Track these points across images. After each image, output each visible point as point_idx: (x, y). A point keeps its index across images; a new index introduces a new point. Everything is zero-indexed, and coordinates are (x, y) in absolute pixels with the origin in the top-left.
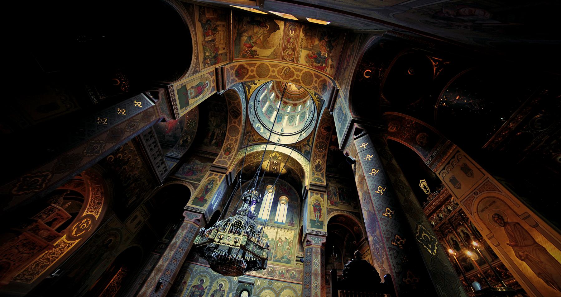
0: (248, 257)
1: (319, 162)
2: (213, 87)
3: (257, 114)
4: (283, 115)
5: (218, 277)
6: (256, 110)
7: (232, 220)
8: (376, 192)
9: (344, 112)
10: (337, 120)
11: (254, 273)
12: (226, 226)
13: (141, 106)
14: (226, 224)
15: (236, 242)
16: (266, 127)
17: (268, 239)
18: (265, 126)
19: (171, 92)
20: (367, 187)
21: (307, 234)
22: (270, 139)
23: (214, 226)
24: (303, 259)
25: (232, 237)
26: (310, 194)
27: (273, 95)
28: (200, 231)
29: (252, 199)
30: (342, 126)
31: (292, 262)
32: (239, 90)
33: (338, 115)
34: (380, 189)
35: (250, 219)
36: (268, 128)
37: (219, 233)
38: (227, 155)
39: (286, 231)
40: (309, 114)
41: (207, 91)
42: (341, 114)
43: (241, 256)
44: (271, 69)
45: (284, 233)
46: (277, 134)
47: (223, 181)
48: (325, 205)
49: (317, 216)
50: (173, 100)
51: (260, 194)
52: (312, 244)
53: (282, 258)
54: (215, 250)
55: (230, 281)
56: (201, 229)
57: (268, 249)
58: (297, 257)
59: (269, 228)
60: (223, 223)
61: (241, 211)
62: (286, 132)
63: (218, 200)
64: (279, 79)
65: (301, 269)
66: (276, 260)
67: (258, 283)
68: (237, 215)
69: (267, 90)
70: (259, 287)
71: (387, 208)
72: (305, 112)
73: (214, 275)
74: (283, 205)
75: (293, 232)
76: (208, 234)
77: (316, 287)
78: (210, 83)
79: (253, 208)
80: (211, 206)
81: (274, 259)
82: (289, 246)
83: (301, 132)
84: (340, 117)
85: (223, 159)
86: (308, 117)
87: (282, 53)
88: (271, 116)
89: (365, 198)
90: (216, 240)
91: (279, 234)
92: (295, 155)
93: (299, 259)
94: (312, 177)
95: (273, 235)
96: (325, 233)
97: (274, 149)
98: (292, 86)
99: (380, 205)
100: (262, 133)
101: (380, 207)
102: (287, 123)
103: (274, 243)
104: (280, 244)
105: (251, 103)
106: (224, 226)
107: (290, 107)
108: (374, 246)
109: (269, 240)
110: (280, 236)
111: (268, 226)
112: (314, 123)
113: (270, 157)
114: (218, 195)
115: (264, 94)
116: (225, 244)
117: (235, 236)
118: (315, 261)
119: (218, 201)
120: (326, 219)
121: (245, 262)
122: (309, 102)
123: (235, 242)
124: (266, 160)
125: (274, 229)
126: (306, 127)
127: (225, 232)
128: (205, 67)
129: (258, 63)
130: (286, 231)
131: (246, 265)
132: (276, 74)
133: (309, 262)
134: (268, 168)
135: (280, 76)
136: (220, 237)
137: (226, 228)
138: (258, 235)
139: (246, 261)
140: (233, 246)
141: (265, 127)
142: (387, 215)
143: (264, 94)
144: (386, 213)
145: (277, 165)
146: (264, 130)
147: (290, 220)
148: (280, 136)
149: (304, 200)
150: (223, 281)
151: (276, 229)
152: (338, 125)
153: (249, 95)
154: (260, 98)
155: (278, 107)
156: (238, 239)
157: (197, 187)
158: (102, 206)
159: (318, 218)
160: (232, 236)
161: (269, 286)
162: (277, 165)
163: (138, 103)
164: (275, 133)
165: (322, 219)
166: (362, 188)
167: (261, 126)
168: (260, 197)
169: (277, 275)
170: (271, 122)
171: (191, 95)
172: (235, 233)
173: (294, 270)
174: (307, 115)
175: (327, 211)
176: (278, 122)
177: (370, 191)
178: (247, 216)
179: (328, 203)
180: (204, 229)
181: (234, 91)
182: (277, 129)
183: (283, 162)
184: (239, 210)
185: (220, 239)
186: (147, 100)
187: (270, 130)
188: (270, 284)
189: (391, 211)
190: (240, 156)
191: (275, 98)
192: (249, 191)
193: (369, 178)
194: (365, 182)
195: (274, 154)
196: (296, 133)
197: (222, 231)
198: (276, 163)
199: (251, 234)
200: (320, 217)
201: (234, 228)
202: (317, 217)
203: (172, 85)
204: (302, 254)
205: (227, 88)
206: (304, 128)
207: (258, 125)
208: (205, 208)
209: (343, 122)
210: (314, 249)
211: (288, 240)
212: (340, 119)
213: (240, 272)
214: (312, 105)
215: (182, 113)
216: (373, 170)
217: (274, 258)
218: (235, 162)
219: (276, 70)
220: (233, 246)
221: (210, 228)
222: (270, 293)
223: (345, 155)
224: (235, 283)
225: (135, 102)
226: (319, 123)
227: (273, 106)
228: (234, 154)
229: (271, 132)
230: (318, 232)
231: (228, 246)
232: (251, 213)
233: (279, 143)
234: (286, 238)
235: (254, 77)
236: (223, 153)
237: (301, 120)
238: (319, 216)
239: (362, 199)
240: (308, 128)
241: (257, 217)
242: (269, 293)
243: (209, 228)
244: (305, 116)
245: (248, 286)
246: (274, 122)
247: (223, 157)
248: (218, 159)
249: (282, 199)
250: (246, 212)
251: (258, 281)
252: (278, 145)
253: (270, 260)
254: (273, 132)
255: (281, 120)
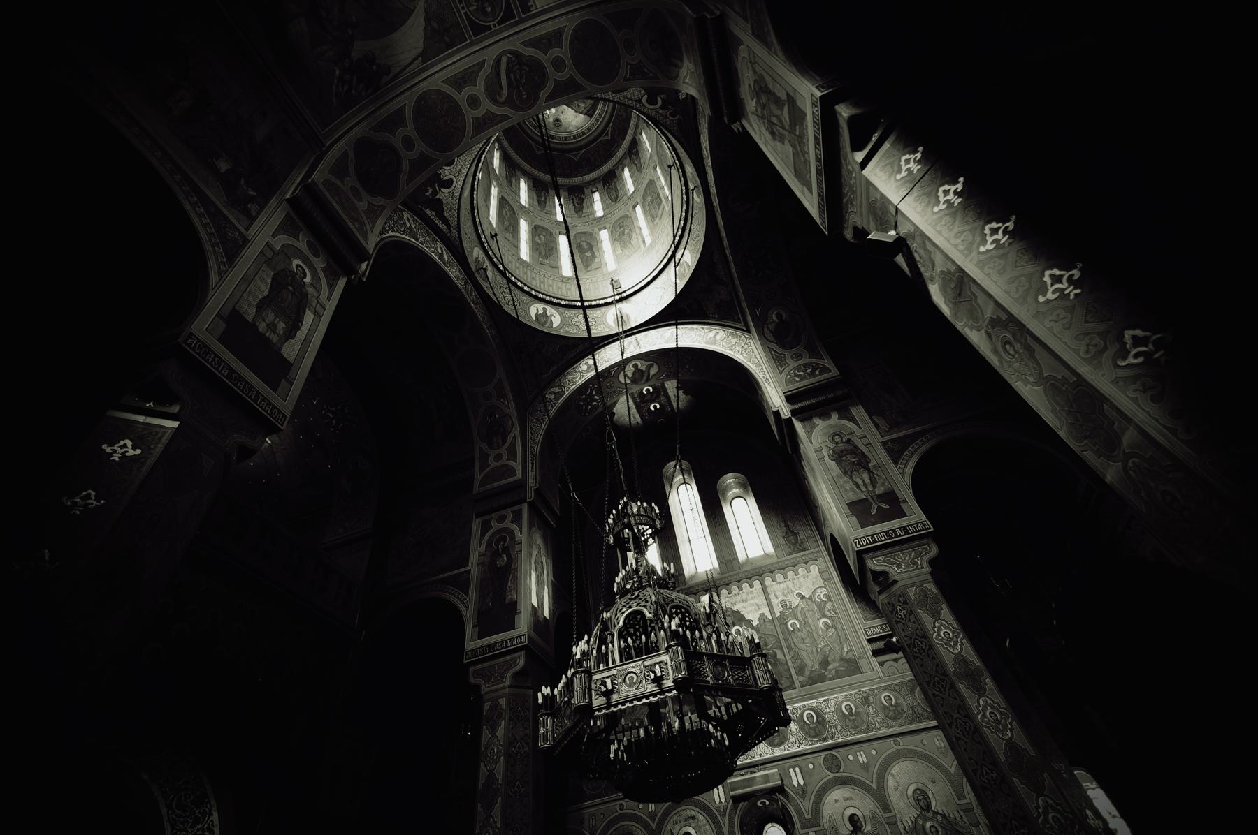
0: (719, 708)
1: (779, 316)
2: (324, 270)
3: (513, 279)
4: (591, 235)
5: (667, 813)
6: (500, 266)
7: (614, 619)
8: (1041, 299)
9: (779, 94)
10: (769, 137)
11: (762, 751)
12: (604, 647)
13: (138, 451)
14: (602, 641)
15: (658, 680)
16: (563, 302)
17: (749, 623)
18: (555, 301)
19: (204, 359)
20: (997, 303)
21: (860, 555)
22: (592, 332)
23: (573, 666)
24: (894, 640)
25: (638, 672)
26: (804, 428)
27: (523, 186)
28: (540, 701)
29: (638, 528)
30: (794, 147)
31: (863, 663)
32: (410, 232)
33: (762, 117)
34: (1055, 279)
35: (662, 591)
36: (570, 303)
37: (595, 677)
38: (499, 448)
39: (790, 574)
40: (666, 180)
41: (316, 294)
42: (773, 106)
43: (695, 717)
44: (461, 97)
45: (789, 583)
46: (606, 304)
47: (531, 525)
48: (870, 439)
49: (860, 482)
50: (229, 378)
51: (653, 504)
52: (897, 578)
53: (825, 663)
54: (612, 737)
55: (706, 809)
56: (539, 694)
57: (764, 656)
58: (869, 641)
59: (735, 589)
60: (591, 642)
61: (625, 580)
62: (627, 284)
63: (546, 584)
64: (505, 118)
65: (907, 676)
66: (810, 678)
67: (796, 779)
68: (620, 598)
69: (494, 183)
70: (802, 792)
71: (1128, 334)
72: (651, 183)
73: (652, 816)
74: (738, 502)
75: (814, 569)
76: (566, 699)
77: (997, 722)
78: (305, 259)
79: (653, 555)
80: (536, 612)
81: (801, 678)
82: (825, 616)
83: (673, 255)
84: (774, 120)
85: (493, 464)
86: (668, 192)
87: (457, 7)
88: (558, 259)
89: (1008, 342)
90: (598, 701)
91: (774, 592)
92: (693, 337)
93: (881, 644)
94: (781, 372)
95: (758, 605)
96: (920, 526)
97: (622, 356)
98: (562, 117)
99: (1087, 334)
100: (561, 326)
101: (1088, 345)
102: (614, 251)
103: (772, 627)
104: (793, 624)
105: (475, 255)
106: (599, 649)
107: (596, 196)
108: (1143, 494)
109: (755, 623)
110: (781, 598)
111: (728, 585)
112: (698, 199)
113: (623, 382)
114: (539, 570)
115: (494, 203)
116: (631, 702)
117: (646, 663)
118: (939, 629)
119: (546, 588)
120: (901, 479)
121: (714, 727)
122: (647, 141)
123: (654, 681)
124: (615, 399)
125: (751, 586)
126: (680, 230)
127: (610, 665)
128: (252, 219)
129: (407, 102)
130: (790, 574)
131: (725, 735)
132: (486, 106)
133: (922, 642)
134: (636, 418)
135: (503, 104)
136: (603, 689)
137: (607, 653)
138: (710, 629)
139: (719, 722)
140: (655, 695)
141: (559, 305)
142: (1140, 360)
143: (494, 203)
144: (1133, 353)
145: (655, 395)
146: (560, 314)
147: (784, 537)
148: (620, 305)
149: (794, 455)
150: (685, 820)
151: (757, 584)
152: (777, 155)
153: (450, 232)
154: (490, 223)
155: (560, 218)
156: (657, 666)
157: (468, 580)
158: (213, 803)
159: (870, 488)
160: (635, 667)
161: (833, 775)
162: (655, 395)
163: (121, 447)
164: (598, 306)
165: (883, 485)
166: (974, 315)
167: (545, 310)
168: (658, 511)
169: (839, 728)
170: (565, 280)
171: (274, 332)
172: (639, 653)
173: (885, 689)
174: (662, 188)
175: (890, 452)
176: (587, 266)
177: (1016, 310)
178: (650, 585)
179: (877, 426)
180: (549, 688)
181: (399, 245)
182: (597, 289)
183: (668, 377)
184: (618, 579)
185: (608, 694)
186: (143, 423)
187: (579, 304)
188: (833, 765)
189: (1154, 334)
190: (539, 431)
191: (535, 197)
192: (614, 512)
193: (986, 268)
194: (974, 289)
195: (630, 370)
196: (661, 266)
197: (602, 668)
198: (651, 390)
199: (688, 632)
200: (873, 482)
201: (629, 640)
202: (865, 485)
203: (191, 334)
204: (881, 626)
205: (371, 244)
206: (674, 237)
207: (535, 309)
208: (523, 626)
209: (792, 131)
210: (912, 593)
211: (810, 598)
212: (778, 129)
213: (720, 768)
214: (661, 146)
215: (286, 400)
216: (991, 229)
217: (798, 674)
218: (532, 453)
219: (479, 89)
220: (655, 695)
221: (564, 679)
222: (851, 798)
223: (856, 242)
224: (725, 810)
225: (108, 450)
226: (713, 190)
227: (546, 225)
228: (518, 434)
229: (584, 308)
230: (894, 530)
231: (638, 703)
232: (654, 572)
233: (625, 329)
234: (803, 597)
235: (424, 162)
236: (485, 446)
237: (652, 217)
238: (868, 481)
239: (995, 351)
240: (687, 230)
241: (683, 574)
242: (846, 799)
243: (561, 678)
244: (659, 196)
245: (767, 803)
246: (576, 271)
247: (491, 458)
248: (482, 471)
249: (727, 486)
250: (641, 577)
251: (791, 770)
252: (627, 336)
253: (792, 686)
254: (591, 307)
255: (594, 256)
